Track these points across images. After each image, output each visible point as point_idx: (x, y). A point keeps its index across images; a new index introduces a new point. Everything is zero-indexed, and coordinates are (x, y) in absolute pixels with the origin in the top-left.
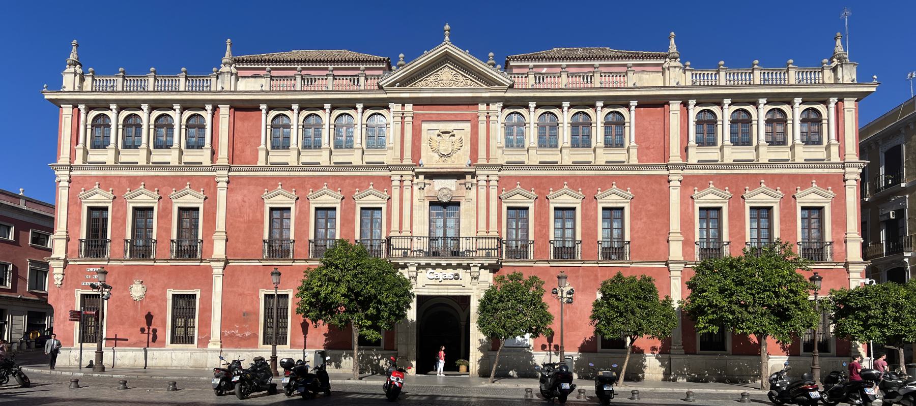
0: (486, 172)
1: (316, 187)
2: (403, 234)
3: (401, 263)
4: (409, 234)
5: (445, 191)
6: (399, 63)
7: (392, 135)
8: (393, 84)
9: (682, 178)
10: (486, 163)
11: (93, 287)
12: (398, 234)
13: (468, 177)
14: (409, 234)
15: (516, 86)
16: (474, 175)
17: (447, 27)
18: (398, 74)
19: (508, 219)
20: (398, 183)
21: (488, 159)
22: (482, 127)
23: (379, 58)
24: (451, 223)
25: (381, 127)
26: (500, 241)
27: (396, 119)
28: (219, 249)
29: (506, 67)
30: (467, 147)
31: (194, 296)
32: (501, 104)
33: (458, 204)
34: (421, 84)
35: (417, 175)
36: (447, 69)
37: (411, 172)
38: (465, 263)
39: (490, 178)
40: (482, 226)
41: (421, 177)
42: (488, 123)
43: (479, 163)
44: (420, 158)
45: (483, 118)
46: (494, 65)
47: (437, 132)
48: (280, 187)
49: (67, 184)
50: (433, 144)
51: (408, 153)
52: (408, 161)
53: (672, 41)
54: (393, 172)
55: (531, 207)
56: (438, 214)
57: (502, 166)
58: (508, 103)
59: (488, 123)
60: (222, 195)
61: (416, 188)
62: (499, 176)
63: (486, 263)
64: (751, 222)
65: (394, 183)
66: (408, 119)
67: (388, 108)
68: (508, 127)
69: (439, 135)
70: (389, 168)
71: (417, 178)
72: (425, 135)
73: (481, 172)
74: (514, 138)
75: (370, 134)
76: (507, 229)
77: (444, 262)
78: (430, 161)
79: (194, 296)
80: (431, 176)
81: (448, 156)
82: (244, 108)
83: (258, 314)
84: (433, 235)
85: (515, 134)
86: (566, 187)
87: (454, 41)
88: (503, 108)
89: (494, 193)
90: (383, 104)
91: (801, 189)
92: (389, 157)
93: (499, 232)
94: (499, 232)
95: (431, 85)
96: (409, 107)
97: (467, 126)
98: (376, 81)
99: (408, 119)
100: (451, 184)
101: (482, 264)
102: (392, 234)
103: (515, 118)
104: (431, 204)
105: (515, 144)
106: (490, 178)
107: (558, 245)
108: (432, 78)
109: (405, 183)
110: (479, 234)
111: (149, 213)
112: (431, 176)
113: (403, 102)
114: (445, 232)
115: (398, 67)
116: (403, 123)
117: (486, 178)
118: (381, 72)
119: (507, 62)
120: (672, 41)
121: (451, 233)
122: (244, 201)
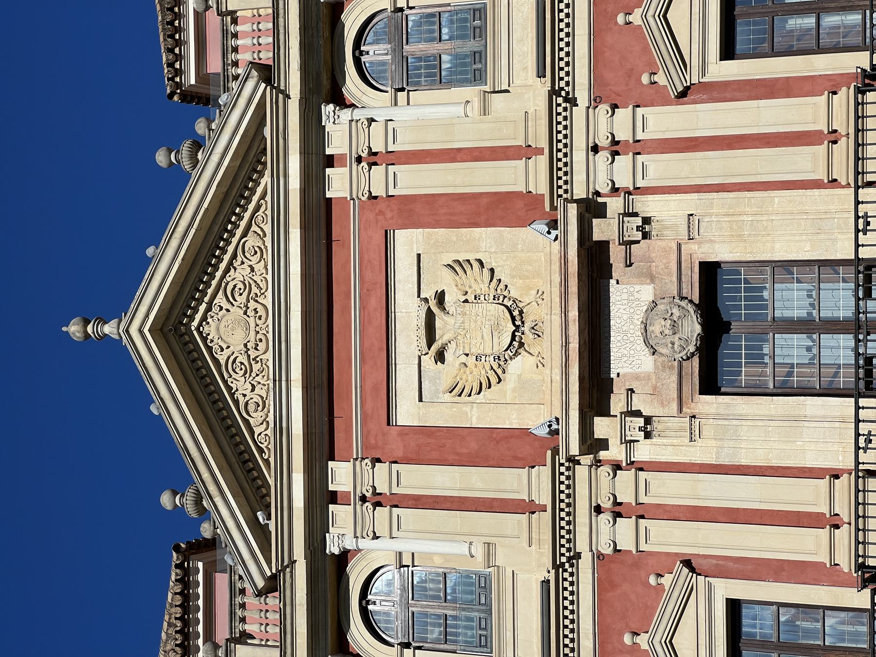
0: (579, 156)
2: (844, 509)
4: (843, 485)
5: (656, 328)
6: (191, 510)
7: (439, 545)
8: (262, 533)
9: (604, 108)
10: (543, 161)
12: (843, 535)
13: (601, 230)
14: (843, 485)
15: (266, 57)
16: (592, 209)
17: (74, 329)
18: (228, 515)
19: (774, 53)
20: (625, 525)
21: (526, 152)
22: (412, 181)
23: (174, 587)
24: (791, 300)
25: (413, 590)
27: (382, 529)
29: (202, 99)
30: (484, 241)
32: (328, 109)
33: (710, 271)
34: (260, 426)
35: (592, 445)
36: (210, 329)
37: (582, 472)
39: (603, 141)
40: (806, 162)
41: (602, 427)
42: (393, 158)
43: (543, 188)
44: (525, 432)
45: (377, 180)
46: (198, 145)
47: (428, 361)
48: (643, 641)
49: (623, 114)
50: (471, 380)
51: (509, 482)
52: (537, 484)
54: (582, 545)
56: (756, 358)
57: (554, 92)
58: (325, 87)
59: (393, 158)
61: (644, 452)
62: (595, 101)
65: (626, 543)
66: (381, 478)
67: (343, 558)
68: (411, 76)
69: (440, 357)
70: (564, 560)
71: (603, 444)
72: (443, 413)
73: (579, 177)
74: (446, 52)
75: (435, 633)
76: (819, 50)
78: (536, 392)
80: (596, 387)
81: (516, 316)
84: (846, 379)
85: (433, 48)
86: (636, 18)
87: (119, 305)
88: (340, 102)
89: (663, 121)
90: (331, 573)
92: (522, 561)
93: (830, 85)
94: (830, 85)
95: (265, 381)
96: (341, 475)
97: (407, 242)
98: (250, 600)
99: (381, 478)
100: (629, 301)
102: (845, 561)
103: (376, 52)
104: (710, 385)
105: (472, 45)
106: (603, 141)
108: (240, 385)
109: (626, 496)
110: (843, 171)
111: (755, 625)
112: (596, 387)
113: (321, 498)
114: (833, 326)
115: (203, 513)
116: (397, 502)
117: (603, 156)
118: (221, 581)
119: (189, 96)
121: (839, 300)
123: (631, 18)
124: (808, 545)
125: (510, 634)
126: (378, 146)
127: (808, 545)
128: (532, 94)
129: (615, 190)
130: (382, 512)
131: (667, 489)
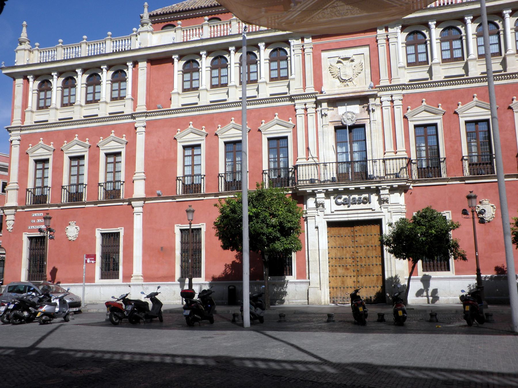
0: (390, 92)
1: (184, 127)
3: (309, 190)
11: (40, 230)
20: (303, 111)
21: (390, 79)
26: (410, 161)
28: (139, 190)
31: (118, 234)
33: (363, 126)
38: (373, 186)
40: (389, 147)
41: (325, 105)
44: (322, 85)
47: (337, 59)
49: (400, 103)
52: (311, 89)
53: (24, 29)
54: (296, 101)
55: (440, 123)
60: (141, 139)
62: (404, 95)
63: (395, 185)
64: (226, 157)
65: (298, 112)
66: (308, 50)
69: (339, 62)
77: (352, 187)
78: (332, 88)
79: (118, 234)
82: (159, 60)
83: (173, 249)
89: (399, 113)
91: (462, 104)
92: (296, 88)
93: (408, 151)
94: (408, 151)
100: (356, 109)
101: (392, 186)
102: (299, 162)
104: (336, 128)
107: (229, 179)
109: (309, 111)
116: (304, 55)
117: (304, 107)
120: (24, 29)
122: (159, 142)
123: (424, 102)
124: (302, 153)
125: (274, 86)
126: (390, 40)
127: (302, 153)
128: (405, 80)
129: (381, 102)
130: (300, 52)
131: (311, 120)
